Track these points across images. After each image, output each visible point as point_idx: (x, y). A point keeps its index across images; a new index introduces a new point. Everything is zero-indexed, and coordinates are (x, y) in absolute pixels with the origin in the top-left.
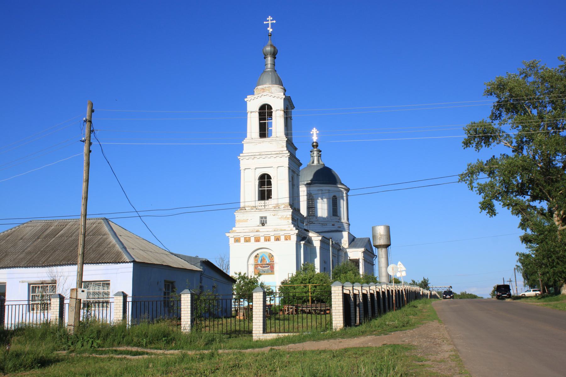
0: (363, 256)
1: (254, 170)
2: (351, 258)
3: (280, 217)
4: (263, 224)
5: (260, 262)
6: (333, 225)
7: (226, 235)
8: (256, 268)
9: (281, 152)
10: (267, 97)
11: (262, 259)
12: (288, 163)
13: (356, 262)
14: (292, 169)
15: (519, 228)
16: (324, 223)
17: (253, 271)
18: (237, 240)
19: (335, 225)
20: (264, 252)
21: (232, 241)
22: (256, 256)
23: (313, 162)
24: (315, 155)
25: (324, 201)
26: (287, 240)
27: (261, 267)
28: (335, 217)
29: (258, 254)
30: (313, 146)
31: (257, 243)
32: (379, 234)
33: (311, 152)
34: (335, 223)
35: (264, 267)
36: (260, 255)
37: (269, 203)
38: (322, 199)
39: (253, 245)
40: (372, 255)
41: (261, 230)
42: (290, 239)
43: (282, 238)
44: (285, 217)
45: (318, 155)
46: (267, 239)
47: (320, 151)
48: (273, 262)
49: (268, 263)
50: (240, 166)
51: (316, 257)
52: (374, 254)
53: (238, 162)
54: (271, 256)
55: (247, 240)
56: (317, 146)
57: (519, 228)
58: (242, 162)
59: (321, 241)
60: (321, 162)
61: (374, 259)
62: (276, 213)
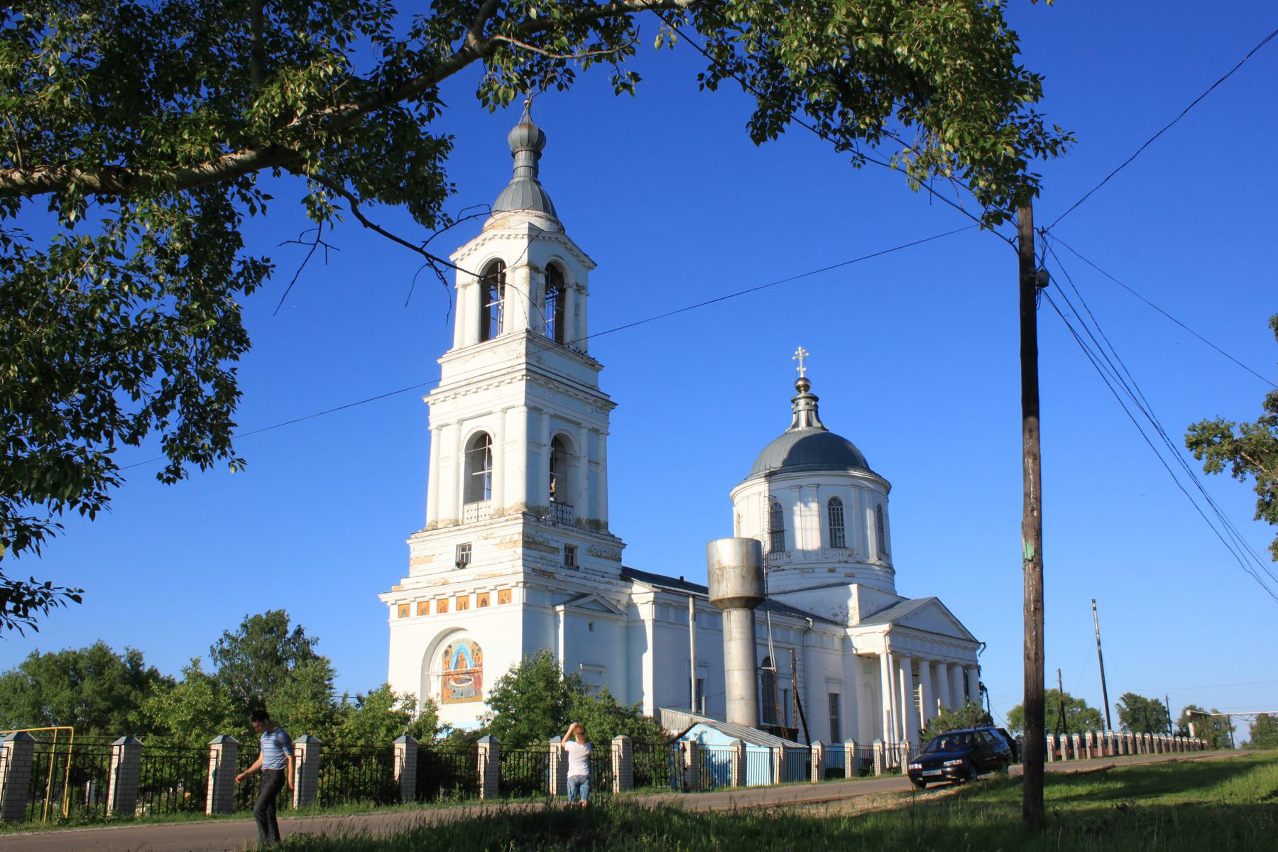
0: (888, 643)
1: (456, 426)
2: (859, 652)
3: (498, 541)
4: (461, 564)
5: (455, 668)
6: (832, 571)
7: (380, 600)
8: (445, 684)
9: (510, 370)
10: (496, 241)
11: (457, 661)
12: (523, 395)
13: (873, 660)
14: (552, 412)
15: (1258, 517)
16: (806, 566)
17: (440, 692)
18: (404, 612)
19: (816, 570)
20: (463, 640)
21: (394, 611)
22: (446, 652)
23: (797, 425)
24: (801, 407)
25: (811, 510)
26: (503, 602)
27: (456, 681)
28: (837, 551)
29: (450, 646)
30: (798, 388)
31: (443, 616)
32: (717, 566)
33: (793, 402)
34: (836, 565)
35: (462, 681)
36: (454, 650)
37: (487, 507)
38: (806, 505)
39: (435, 623)
40: (970, 645)
41: (451, 581)
42: (510, 599)
43: (493, 598)
44: (508, 540)
45: (807, 407)
46: (462, 605)
47: (816, 399)
48: (481, 665)
49: (469, 668)
50: (428, 420)
51: (645, 649)
52: (977, 642)
53: (426, 409)
54: (477, 651)
55: (423, 611)
56: (807, 387)
57: (1258, 517)
58: (434, 411)
59: (655, 602)
60: (815, 423)
61: (978, 652)
62: (490, 532)
